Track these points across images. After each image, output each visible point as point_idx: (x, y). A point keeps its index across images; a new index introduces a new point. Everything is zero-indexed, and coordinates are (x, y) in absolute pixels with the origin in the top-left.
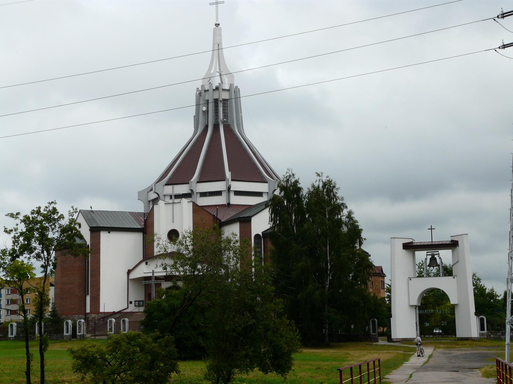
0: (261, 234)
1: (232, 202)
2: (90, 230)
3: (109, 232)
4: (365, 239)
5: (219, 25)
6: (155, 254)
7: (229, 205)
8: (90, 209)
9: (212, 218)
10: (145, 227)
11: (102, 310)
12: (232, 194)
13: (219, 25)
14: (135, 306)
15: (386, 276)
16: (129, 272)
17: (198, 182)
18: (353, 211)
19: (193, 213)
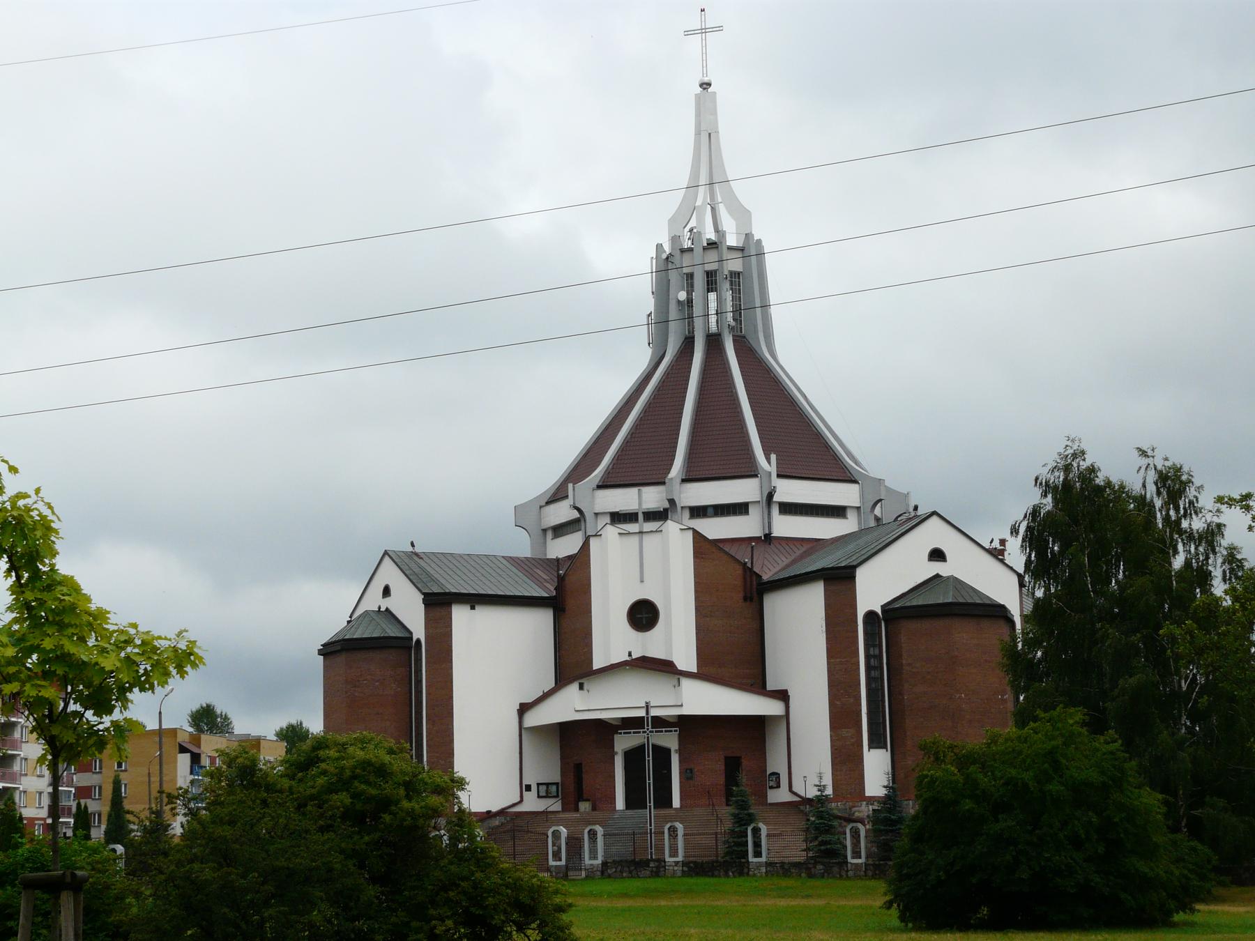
0: (879, 612)
1: (776, 533)
2: (424, 601)
3: (473, 608)
4: (630, 654)
5: (709, 84)
7: (768, 538)
8: (411, 549)
9: (739, 571)
10: (562, 595)
12: (775, 510)
13: (709, 84)
14: (539, 797)
16: (524, 709)
17: (684, 481)
18: (1237, 543)
19: (695, 557)
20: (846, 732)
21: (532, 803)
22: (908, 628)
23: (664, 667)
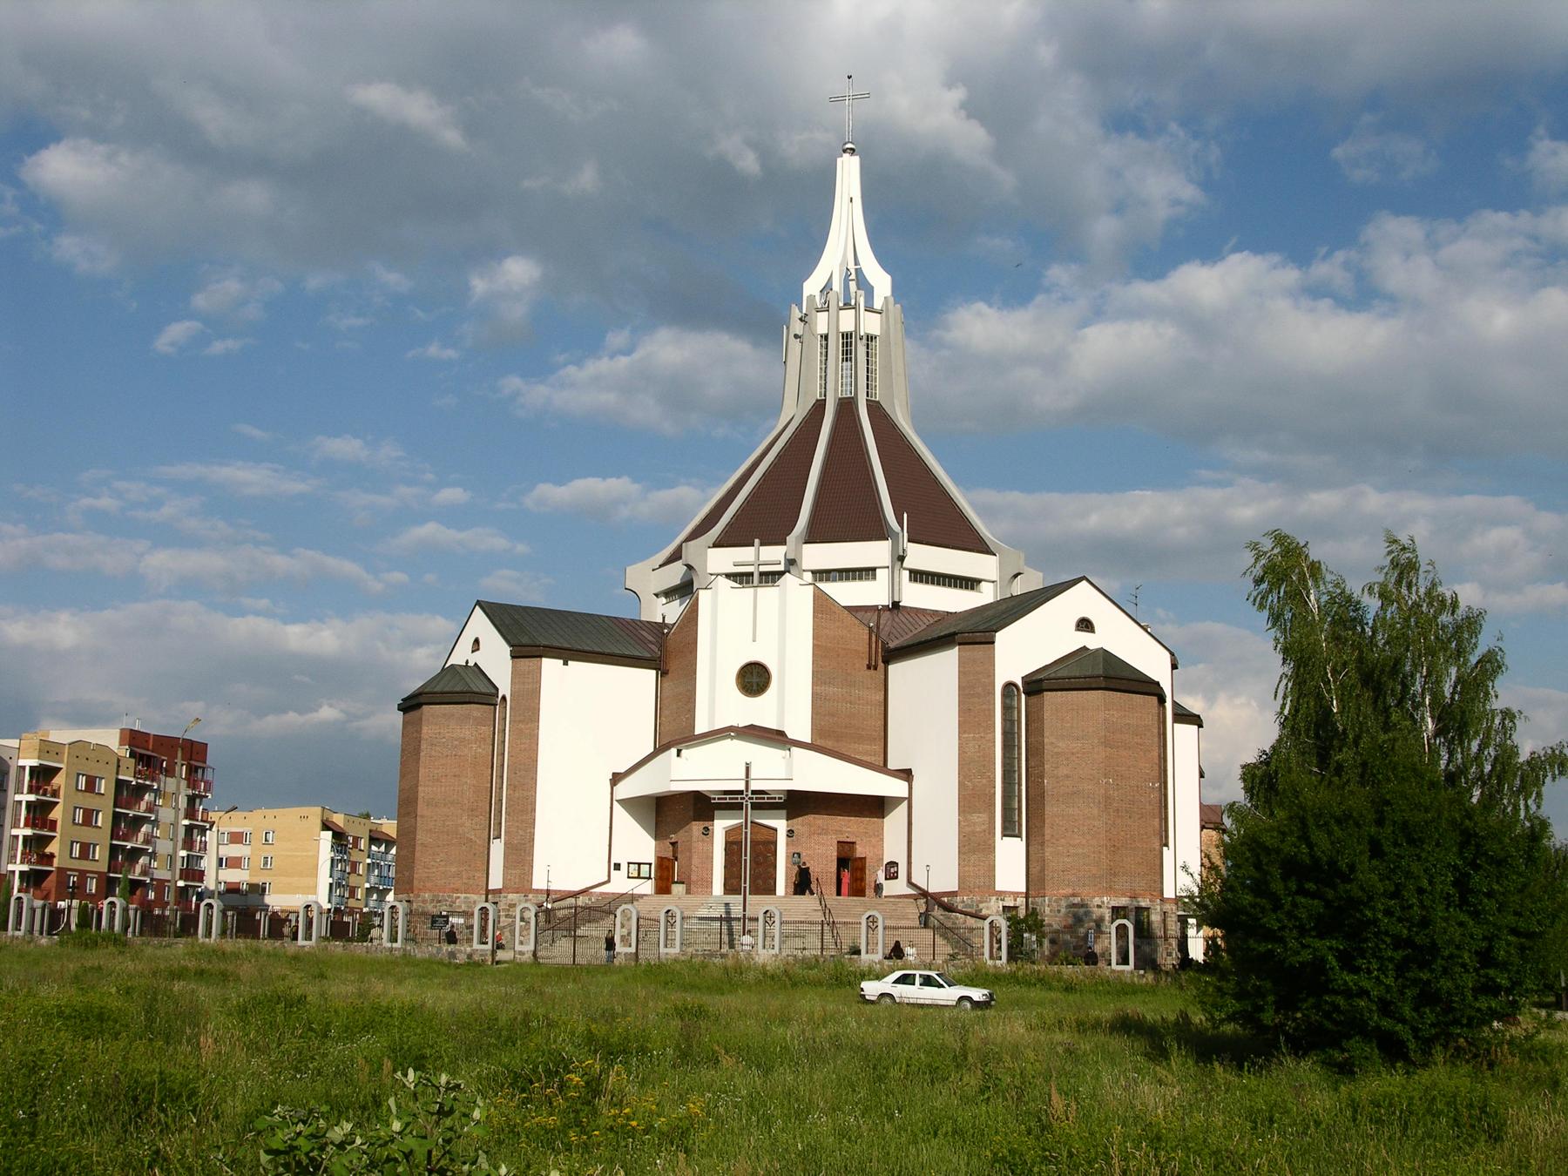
0: (1020, 684)
7: (896, 605)
11: (539, 883)
20: (975, 818)
21: (621, 884)
22: (1052, 700)
23: (776, 738)
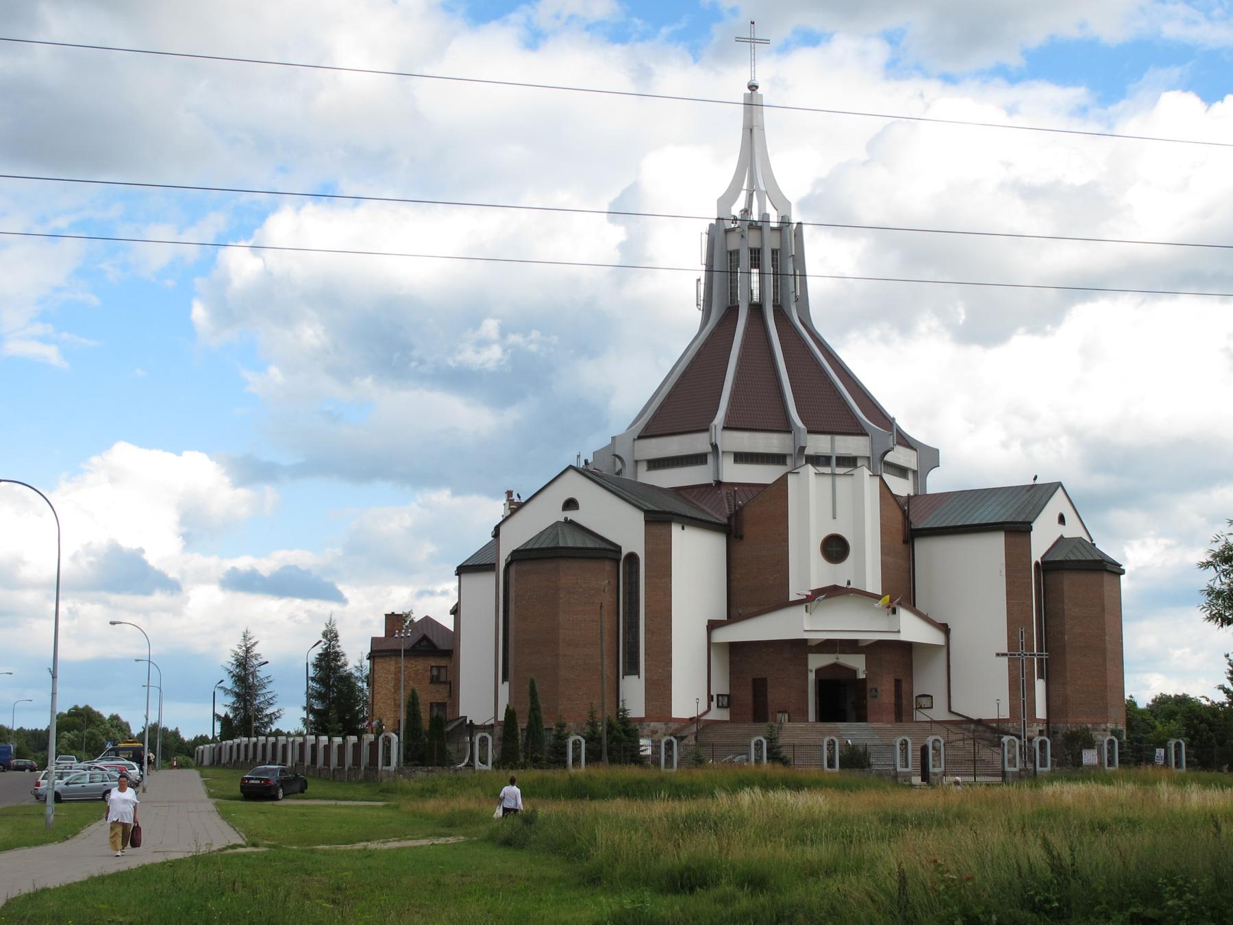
1: (726, 478)
2: (647, 522)
4: (849, 583)
6: (791, 599)
7: (719, 484)
15: (1123, 572)
17: (725, 428)
21: (716, 714)
